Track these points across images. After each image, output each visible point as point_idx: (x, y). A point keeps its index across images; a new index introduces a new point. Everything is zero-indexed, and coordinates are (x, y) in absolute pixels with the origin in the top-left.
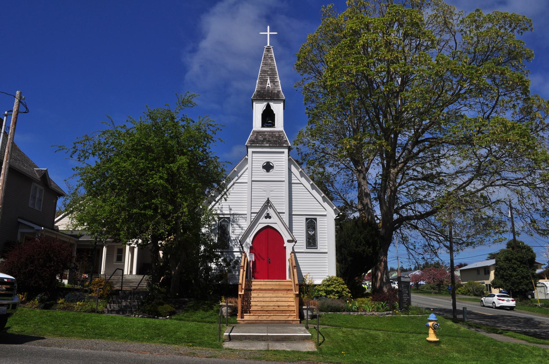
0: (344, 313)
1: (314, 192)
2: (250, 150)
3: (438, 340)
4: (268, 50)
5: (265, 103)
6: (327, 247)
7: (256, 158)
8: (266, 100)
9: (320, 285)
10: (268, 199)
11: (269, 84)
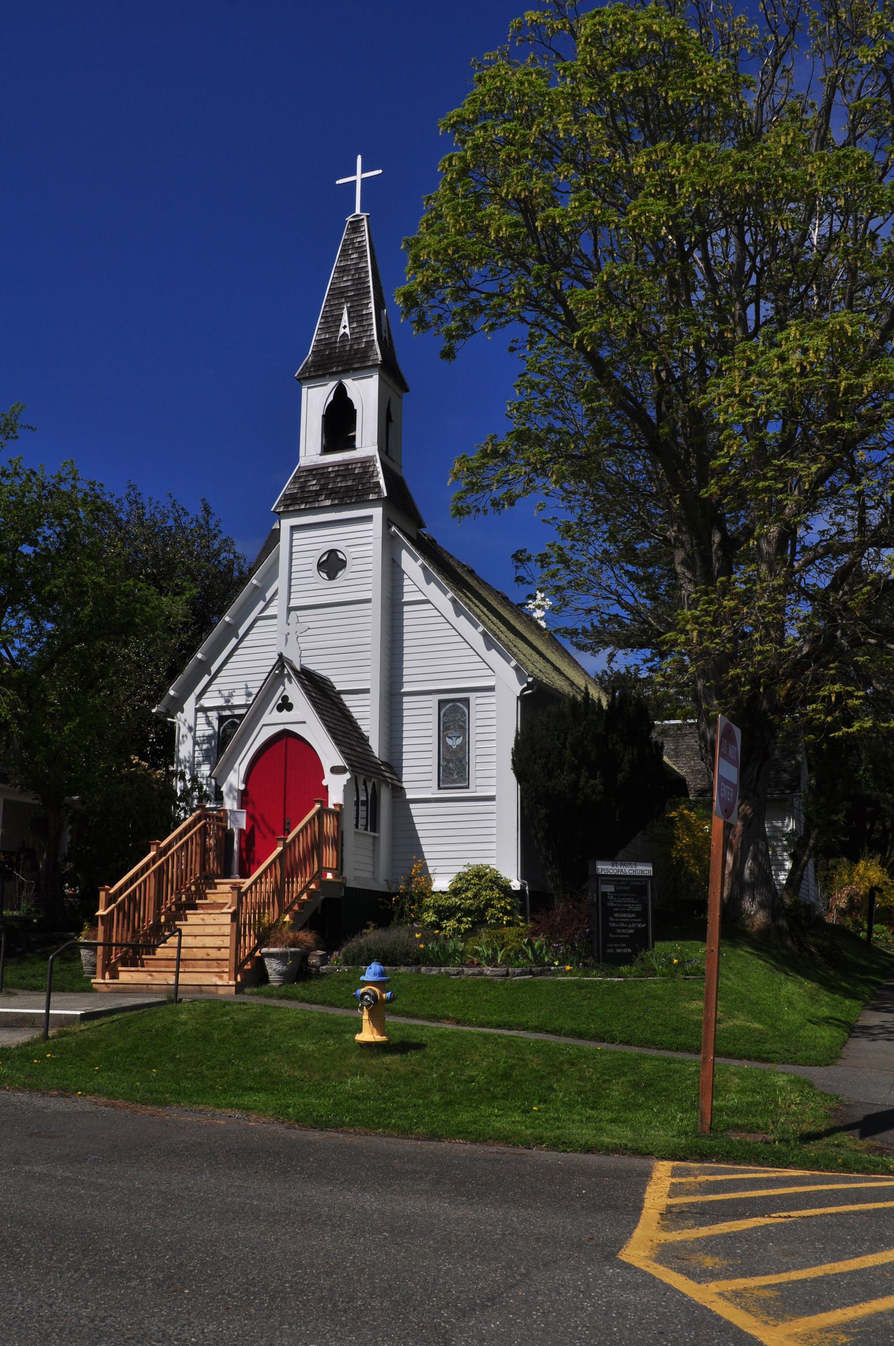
0: (403, 969)
1: (462, 623)
2: (286, 524)
3: (384, 1038)
4: (356, 226)
6: (493, 781)
7: (301, 543)
8: (333, 375)
9: (444, 893)
10: (281, 656)
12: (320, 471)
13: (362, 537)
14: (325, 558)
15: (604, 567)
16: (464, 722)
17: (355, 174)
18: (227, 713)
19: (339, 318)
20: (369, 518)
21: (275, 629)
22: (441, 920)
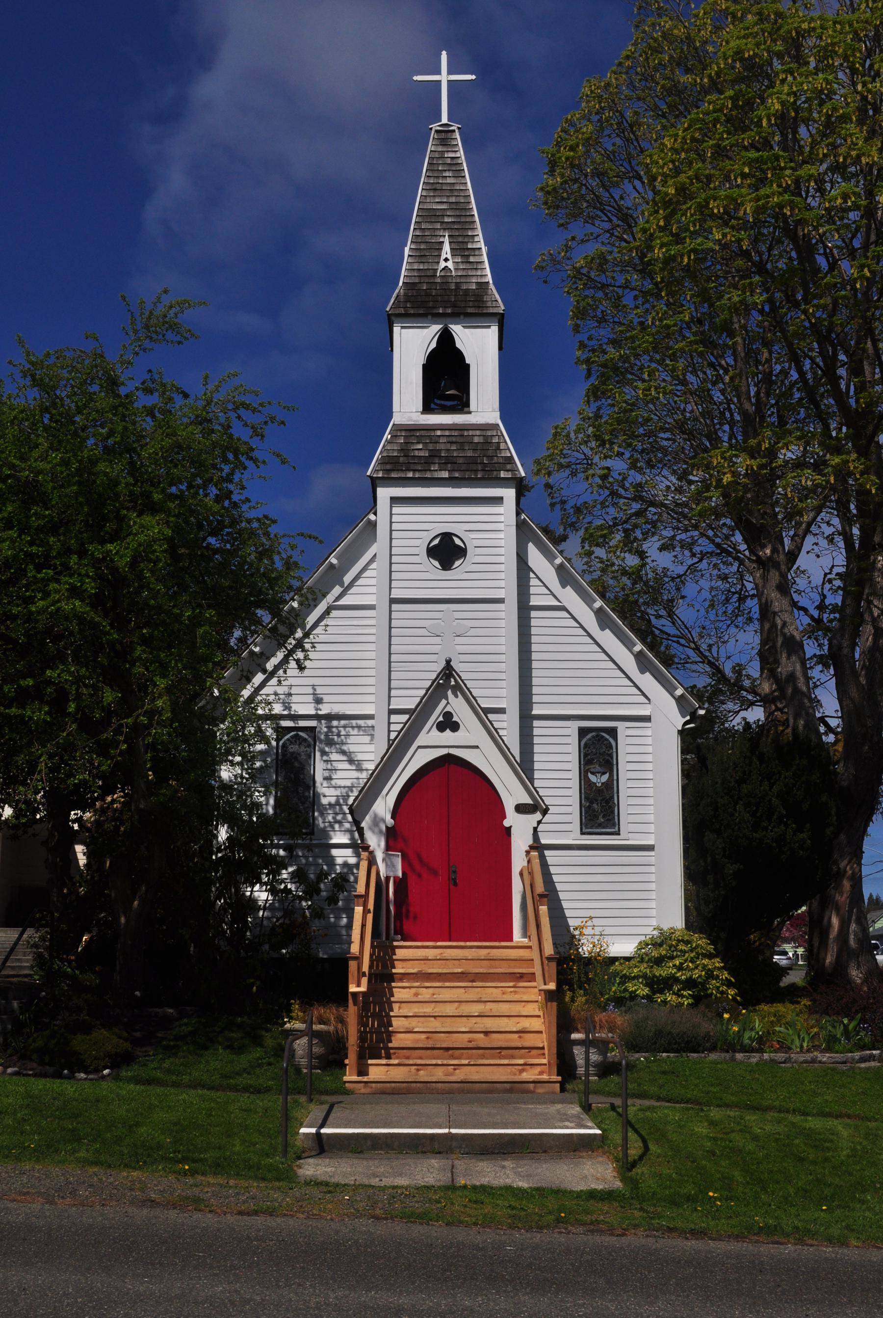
1: (608, 638)
2: (384, 494)
4: (445, 137)
5: (436, 328)
6: (651, 828)
7: (404, 521)
10: (448, 662)
11: (447, 260)
12: (423, 433)
13: (491, 523)
14: (436, 542)
15: (841, 592)
16: (611, 756)
17: (439, 73)
18: (285, 723)
19: (440, 246)
20: (499, 500)
21: (373, 622)
22: (654, 993)
